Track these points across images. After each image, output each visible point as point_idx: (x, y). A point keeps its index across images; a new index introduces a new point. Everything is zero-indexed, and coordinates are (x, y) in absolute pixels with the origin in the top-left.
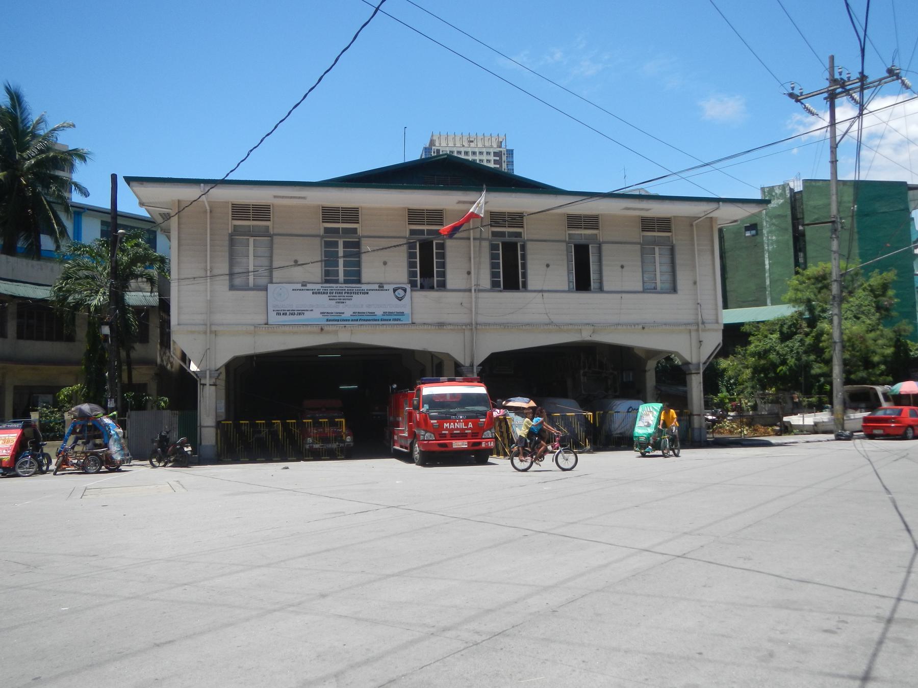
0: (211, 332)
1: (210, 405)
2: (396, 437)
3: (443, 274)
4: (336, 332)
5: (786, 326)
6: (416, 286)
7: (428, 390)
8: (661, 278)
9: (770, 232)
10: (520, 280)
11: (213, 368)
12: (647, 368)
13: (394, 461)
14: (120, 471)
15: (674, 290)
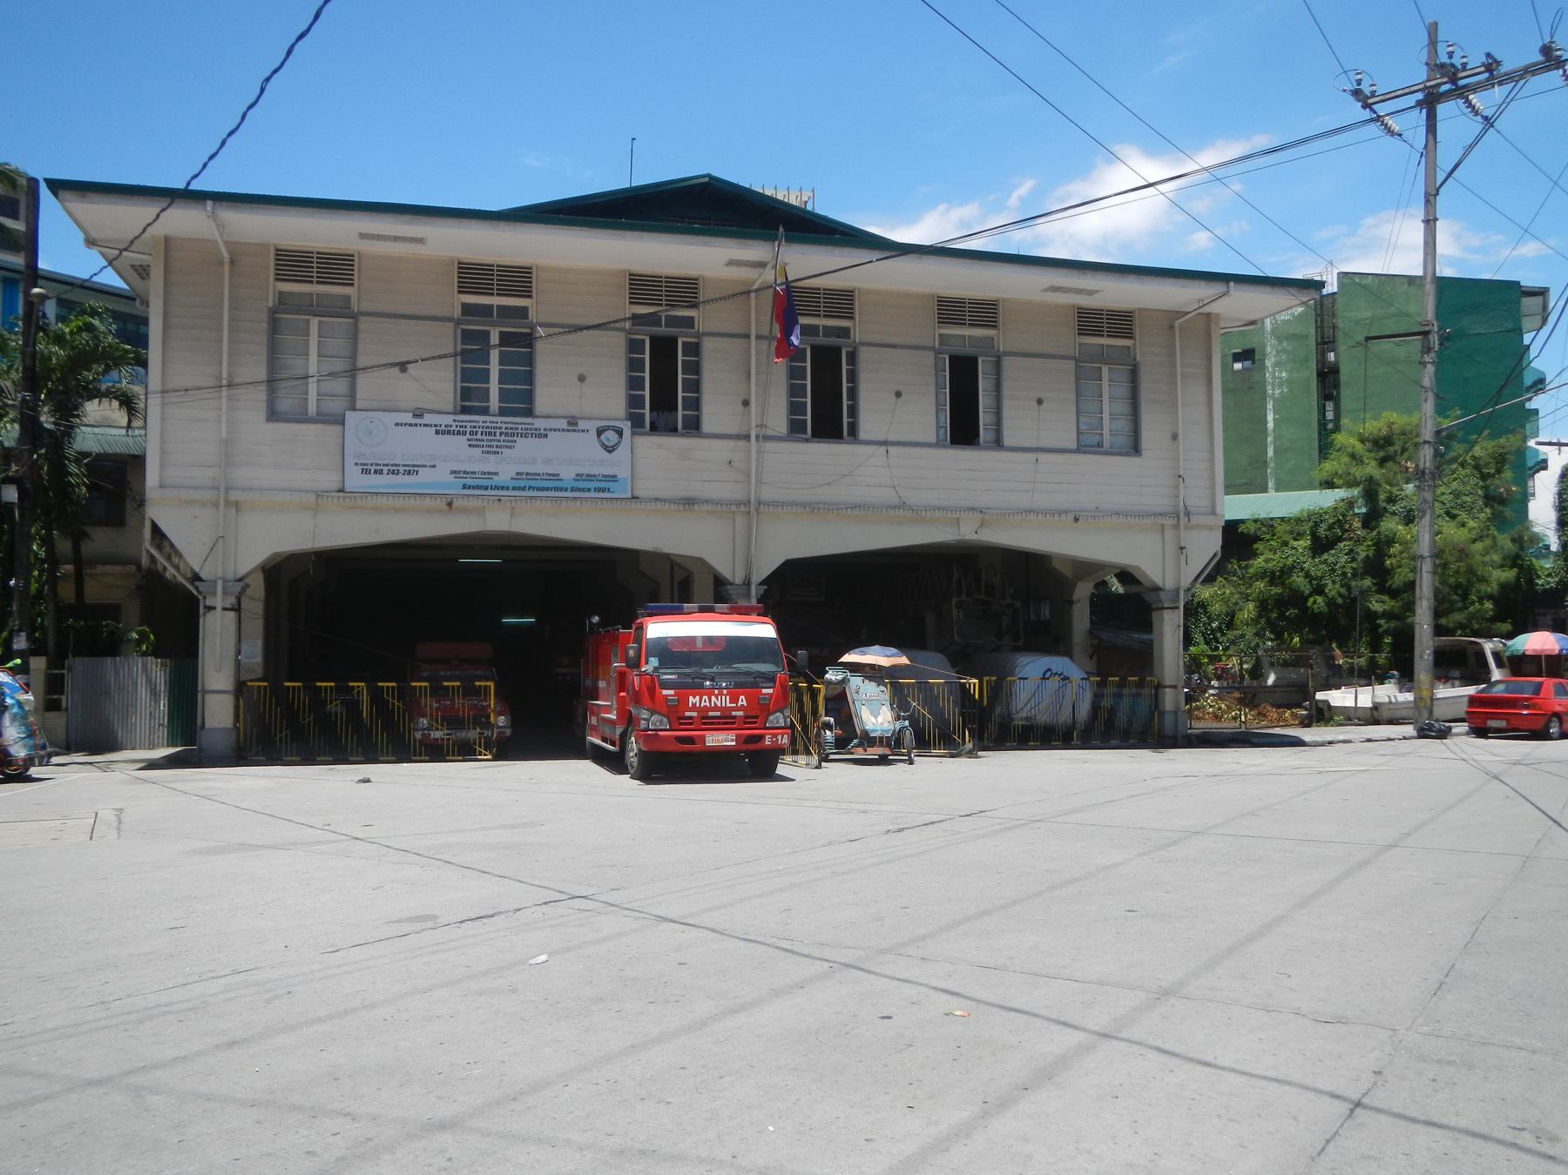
0: (228, 503)
1: (225, 651)
2: (594, 721)
3: (695, 404)
4: (481, 511)
5: (1324, 526)
6: (642, 425)
7: (657, 629)
8: (1112, 426)
9: (1277, 364)
10: (845, 420)
11: (231, 576)
12: (1075, 597)
13: (586, 767)
14: (30, 780)
15: (1135, 449)
